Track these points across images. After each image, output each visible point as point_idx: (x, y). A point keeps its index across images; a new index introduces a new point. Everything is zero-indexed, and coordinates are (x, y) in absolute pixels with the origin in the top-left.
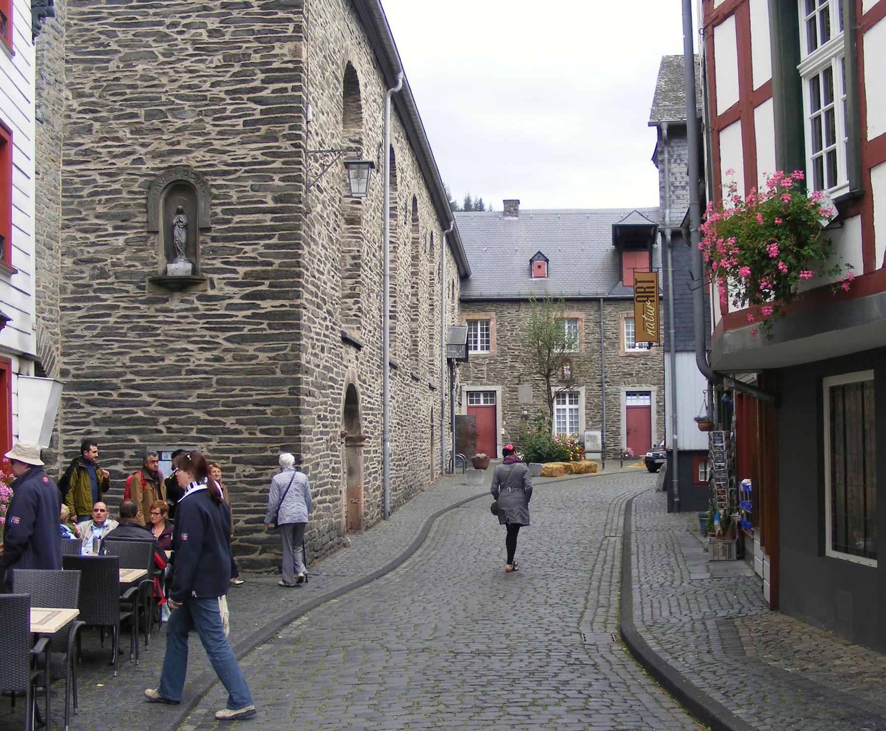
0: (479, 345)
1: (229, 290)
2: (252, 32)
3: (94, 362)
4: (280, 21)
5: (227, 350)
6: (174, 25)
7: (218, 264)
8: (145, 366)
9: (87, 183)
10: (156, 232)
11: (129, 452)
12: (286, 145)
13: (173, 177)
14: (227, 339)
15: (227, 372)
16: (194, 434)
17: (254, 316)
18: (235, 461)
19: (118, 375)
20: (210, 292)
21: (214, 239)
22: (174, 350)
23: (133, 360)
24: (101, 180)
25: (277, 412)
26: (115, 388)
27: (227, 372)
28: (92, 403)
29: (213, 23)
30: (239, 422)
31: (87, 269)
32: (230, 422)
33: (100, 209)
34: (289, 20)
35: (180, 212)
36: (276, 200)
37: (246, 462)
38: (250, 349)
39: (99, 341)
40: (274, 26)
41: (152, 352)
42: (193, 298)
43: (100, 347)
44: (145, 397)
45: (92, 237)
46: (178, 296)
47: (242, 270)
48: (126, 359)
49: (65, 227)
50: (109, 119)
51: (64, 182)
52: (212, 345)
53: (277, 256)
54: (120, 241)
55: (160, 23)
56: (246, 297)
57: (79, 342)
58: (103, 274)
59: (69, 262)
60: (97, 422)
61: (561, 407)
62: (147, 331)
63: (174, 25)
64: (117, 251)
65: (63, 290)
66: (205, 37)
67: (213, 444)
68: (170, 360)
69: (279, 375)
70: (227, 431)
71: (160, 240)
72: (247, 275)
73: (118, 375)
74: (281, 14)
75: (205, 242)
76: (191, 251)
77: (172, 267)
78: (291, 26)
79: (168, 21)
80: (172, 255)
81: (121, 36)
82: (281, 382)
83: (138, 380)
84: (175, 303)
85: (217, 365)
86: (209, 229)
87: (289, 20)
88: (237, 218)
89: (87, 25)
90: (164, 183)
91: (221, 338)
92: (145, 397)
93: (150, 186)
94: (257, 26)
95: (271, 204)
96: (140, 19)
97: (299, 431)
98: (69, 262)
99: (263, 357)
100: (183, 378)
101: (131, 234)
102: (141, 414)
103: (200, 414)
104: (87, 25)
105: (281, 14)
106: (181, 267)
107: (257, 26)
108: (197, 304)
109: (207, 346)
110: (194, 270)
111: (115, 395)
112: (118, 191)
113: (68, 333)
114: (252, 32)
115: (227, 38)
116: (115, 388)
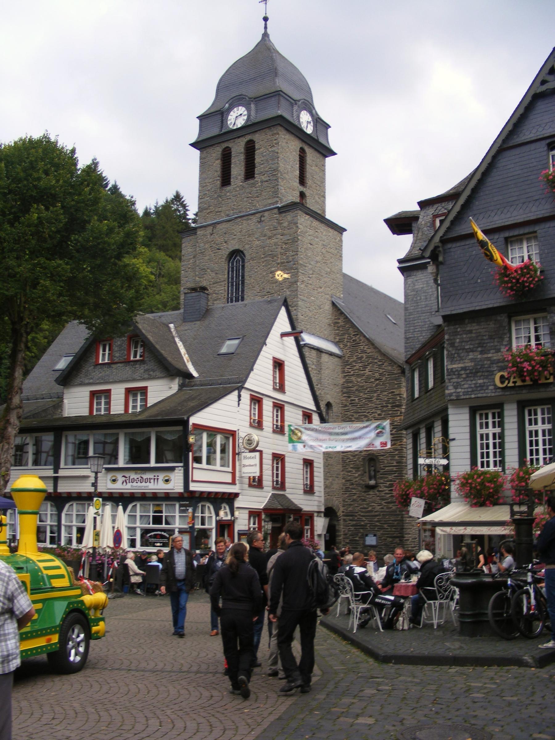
0: (491, 459)
1: (385, 489)
2: (389, 414)
3: (350, 509)
4: (396, 410)
5: (385, 506)
6: (368, 413)
7: (382, 481)
8: (364, 510)
9: (348, 458)
10: (366, 472)
11: (360, 534)
12: (399, 447)
13: (370, 457)
14: (385, 503)
15: (384, 512)
16: (376, 529)
17: (391, 496)
18: (387, 537)
19: (357, 513)
20: (380, 489)
21: (381, 474)
22: (371, 506)
23: (361, 508)
24: (351, 458)
25: (398, 523)
26: (356, 516)
27: (384, 512)
28: (351, 520)
29: (379, 412)
30: (388, 526)
31: (348, 483)
32: (385, 526)
33: (351, 466)
34: (398, 410)
35: (372, 466)
36: (397, 463)
37: (390, 537)
38: (391, 505)
39: (352, 503)
40: (394, 412)
41: (365, 506)
42: (376, 491)
43: (352, 505)
44: (364, 519)
45: (349, 474)
46: (372, 490)
47: (388, 483)
48: (359, 508)
49: (343, 471)
50: (519, 483)
51: (343, 458)
52: (381, 504)
53: (397, 479)
54: (357, 475)
55: (365, 412)
56: (389, 491)
57: (346, 503)
58: (352, 484)
59: (344, 481)
60: (352, 526)
61: (484, 431)
62: (364, 500)
63: (368, 413)
64: (356, 478)
65: (342, 489)
66: (377, 416)
67: (381, 532)
68: (370, 509)
69: (398, 513)
70: (385, 529)
71: (367, 474)
72: (390, 484)
73: (357, 513)
74: (396, 409)
75: (379, 475)
76: (375, 477)
77: (370, 482)
78: (399, 412)
79: (367, 411)
80: (370, 479)
81: (355, 416)
82: (398, 515)
83: (362, 514)
84: (371, 493)
85: (382, 510)
86: (379, 472)
87: (398, 410)
88: (387, 468)
89: (346, 413)
90: (367, 458)
91: (383, 502)
92: (364, 519)
93: (364, 459)
94: (390, 412)
95: (395, 464)
96: (360, 411)
97: (403, 529)
98: (344, 481)
99: (394, 507)
100: (373, 513)
101: (359, 473)
102: (363, 523)
103: (377, 524)
104: (346, 413)
105: (396, 409)
106: (372, 482)
107: (390, 412)
108: (377, 493)
109: (380, 504)
110: (376, 483)
111: (356, 518)
112: (355, 461)
113: (344, 501)
114: (389, 414)
115: (382, 416)
116: (356, 516)
